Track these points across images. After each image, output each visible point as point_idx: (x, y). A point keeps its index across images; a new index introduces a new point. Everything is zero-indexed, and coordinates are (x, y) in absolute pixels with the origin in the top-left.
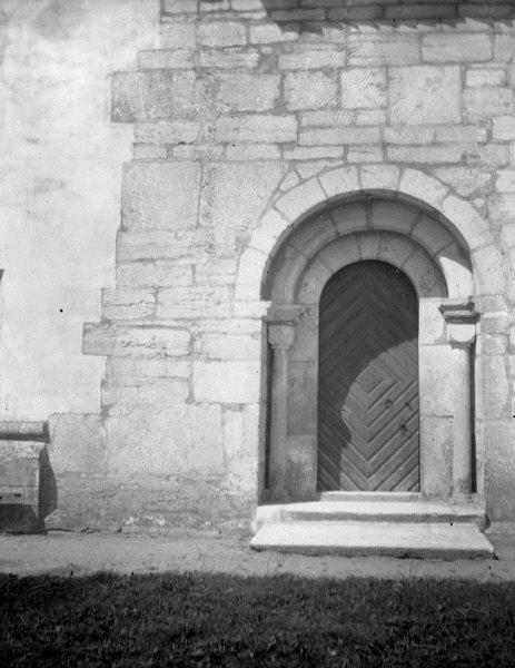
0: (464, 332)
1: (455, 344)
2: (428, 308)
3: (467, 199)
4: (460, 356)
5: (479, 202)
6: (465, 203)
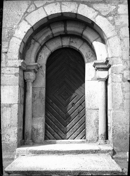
0: (103, 74)
1: (99, 79)
2: (89, 68)
3: (105, 17)
4: (102, 84)
5: (111, 18)
6: (105, 18)
